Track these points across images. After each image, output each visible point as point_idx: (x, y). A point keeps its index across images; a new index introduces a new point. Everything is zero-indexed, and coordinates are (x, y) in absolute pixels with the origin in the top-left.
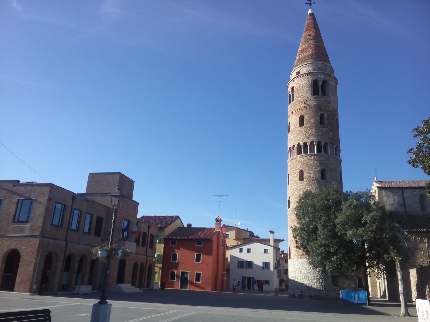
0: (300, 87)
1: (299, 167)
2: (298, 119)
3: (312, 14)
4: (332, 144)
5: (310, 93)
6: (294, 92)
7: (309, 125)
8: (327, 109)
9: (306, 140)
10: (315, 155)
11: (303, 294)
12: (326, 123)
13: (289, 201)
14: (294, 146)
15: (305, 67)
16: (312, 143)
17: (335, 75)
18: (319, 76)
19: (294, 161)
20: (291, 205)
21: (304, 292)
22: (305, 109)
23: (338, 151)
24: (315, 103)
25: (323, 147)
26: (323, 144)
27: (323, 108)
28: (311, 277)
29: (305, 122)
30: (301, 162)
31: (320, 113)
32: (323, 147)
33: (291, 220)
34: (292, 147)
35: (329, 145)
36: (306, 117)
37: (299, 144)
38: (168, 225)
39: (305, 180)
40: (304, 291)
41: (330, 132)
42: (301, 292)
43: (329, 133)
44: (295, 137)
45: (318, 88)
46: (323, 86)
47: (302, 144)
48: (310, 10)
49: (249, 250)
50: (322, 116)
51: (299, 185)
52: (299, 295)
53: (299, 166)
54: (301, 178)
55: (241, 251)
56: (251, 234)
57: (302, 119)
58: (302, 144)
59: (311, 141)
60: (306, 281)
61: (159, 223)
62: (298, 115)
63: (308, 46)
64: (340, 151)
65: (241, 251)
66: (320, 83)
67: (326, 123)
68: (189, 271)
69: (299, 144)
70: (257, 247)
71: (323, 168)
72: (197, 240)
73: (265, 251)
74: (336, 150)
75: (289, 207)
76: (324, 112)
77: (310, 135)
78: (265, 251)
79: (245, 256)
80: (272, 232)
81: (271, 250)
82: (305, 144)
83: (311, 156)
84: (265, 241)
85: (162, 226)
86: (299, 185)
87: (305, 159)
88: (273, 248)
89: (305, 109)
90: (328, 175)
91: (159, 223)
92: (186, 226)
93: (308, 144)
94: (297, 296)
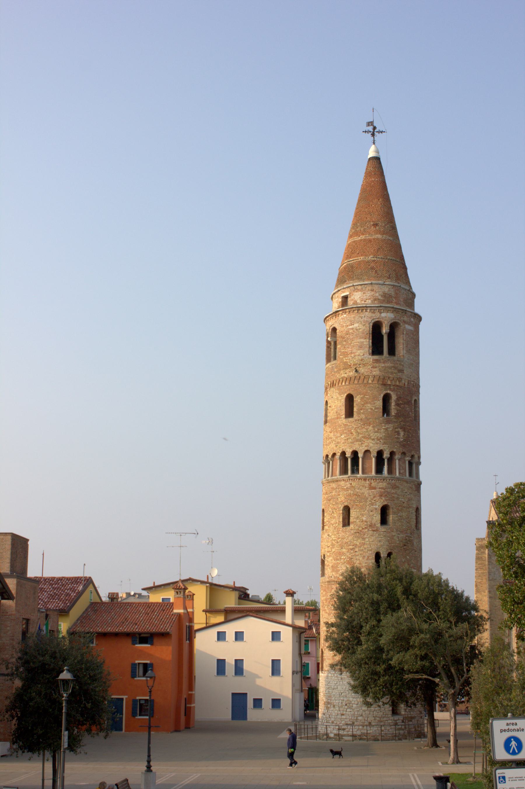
0: (347, 333)
1: (342, 500)
2: (343, 401)
3: (377, 159)
4: (404, 453)
5: (367, 349)
6: (336, 337)
7: (363, 416)
8: (398, 383)
9: (356, 447)
10: (372, 478)
11: (341, 732)
12: (393, 414)
13: (323, 562)
14: (334, 455)
15: (358, 290)
16: (367, 452)
17: (418, 309)
18: (383, 315)
19: (334, 485)
20: (326, 572)
21: (344, 729)
22: (356, 382)
23: (414, 466)
24: (376, 372)
25: (386, 461)
26: (386, 455)
27: (389, 383)
28: (356, 703)
29: (355, 409)
30: (347, 489)
31: (385, 392)
32: (386, 461)
33: (326, 600)
34: (330, 456)
35: (397, 457)
36: (357, 400)
37: (343, 453)
38: (74, 603)
39: (352, 526)
40: (345, 727)
41: (400, 430)
42: (339, 729)
43: (398, 434)
44: (337, 438)
45: (358, 458)
46: (392, 335)
47: (348, 455)
48: (373, 148)
49: (239, 636)
50: (386, 399)
51: (341, 534)
52: (335, 735)
53: (343, 498)
54: (346, 522)
55: (221, 636)
56: (243, 594)
57: (350, 399)
58: (348, 455)
59: (366, 449)
60: (348, 710)
61: (52, 597)
62: (343, 393)
63: (365, 240)
64: (419, 463)
65: (221, 636)
66: (385, 330)
67: (393, 412)
68: (125, 697)
69: (343, 453)
70: (255, 627)
71: (385, 503)
72: (140, 634)
73: (276, 636)
74: (410, 464)
75: (323, 574)
76: (390, 389)
77: (364, 437)
78: (276, 636)
79: (229, 651)
80: (290, 594)
81: (287, 634)
82: (355, 454)
83: (365, 480)
84: (268, 610)
85: (61, 606)
86: (341, 534)
87: (354, 484)
88: (291, 629)
89: (356, 382)
90: (391, 518)
91: (52, 597)
92: (105, 598)
93: (360, 455)
94: (332, 735)
